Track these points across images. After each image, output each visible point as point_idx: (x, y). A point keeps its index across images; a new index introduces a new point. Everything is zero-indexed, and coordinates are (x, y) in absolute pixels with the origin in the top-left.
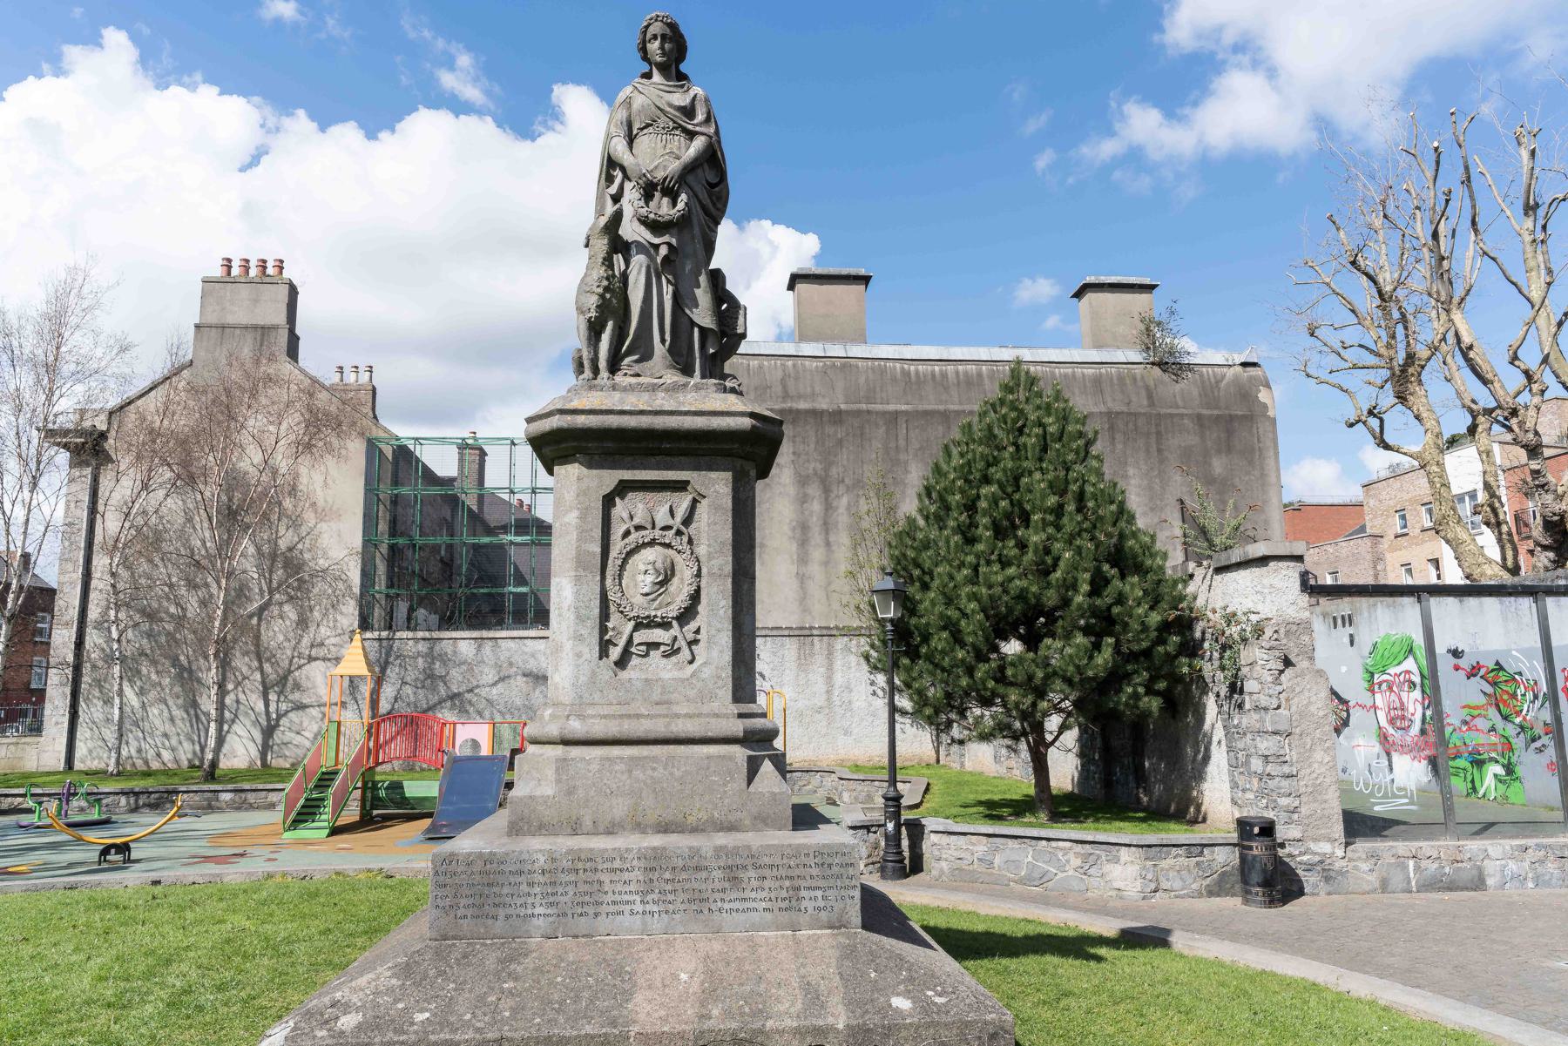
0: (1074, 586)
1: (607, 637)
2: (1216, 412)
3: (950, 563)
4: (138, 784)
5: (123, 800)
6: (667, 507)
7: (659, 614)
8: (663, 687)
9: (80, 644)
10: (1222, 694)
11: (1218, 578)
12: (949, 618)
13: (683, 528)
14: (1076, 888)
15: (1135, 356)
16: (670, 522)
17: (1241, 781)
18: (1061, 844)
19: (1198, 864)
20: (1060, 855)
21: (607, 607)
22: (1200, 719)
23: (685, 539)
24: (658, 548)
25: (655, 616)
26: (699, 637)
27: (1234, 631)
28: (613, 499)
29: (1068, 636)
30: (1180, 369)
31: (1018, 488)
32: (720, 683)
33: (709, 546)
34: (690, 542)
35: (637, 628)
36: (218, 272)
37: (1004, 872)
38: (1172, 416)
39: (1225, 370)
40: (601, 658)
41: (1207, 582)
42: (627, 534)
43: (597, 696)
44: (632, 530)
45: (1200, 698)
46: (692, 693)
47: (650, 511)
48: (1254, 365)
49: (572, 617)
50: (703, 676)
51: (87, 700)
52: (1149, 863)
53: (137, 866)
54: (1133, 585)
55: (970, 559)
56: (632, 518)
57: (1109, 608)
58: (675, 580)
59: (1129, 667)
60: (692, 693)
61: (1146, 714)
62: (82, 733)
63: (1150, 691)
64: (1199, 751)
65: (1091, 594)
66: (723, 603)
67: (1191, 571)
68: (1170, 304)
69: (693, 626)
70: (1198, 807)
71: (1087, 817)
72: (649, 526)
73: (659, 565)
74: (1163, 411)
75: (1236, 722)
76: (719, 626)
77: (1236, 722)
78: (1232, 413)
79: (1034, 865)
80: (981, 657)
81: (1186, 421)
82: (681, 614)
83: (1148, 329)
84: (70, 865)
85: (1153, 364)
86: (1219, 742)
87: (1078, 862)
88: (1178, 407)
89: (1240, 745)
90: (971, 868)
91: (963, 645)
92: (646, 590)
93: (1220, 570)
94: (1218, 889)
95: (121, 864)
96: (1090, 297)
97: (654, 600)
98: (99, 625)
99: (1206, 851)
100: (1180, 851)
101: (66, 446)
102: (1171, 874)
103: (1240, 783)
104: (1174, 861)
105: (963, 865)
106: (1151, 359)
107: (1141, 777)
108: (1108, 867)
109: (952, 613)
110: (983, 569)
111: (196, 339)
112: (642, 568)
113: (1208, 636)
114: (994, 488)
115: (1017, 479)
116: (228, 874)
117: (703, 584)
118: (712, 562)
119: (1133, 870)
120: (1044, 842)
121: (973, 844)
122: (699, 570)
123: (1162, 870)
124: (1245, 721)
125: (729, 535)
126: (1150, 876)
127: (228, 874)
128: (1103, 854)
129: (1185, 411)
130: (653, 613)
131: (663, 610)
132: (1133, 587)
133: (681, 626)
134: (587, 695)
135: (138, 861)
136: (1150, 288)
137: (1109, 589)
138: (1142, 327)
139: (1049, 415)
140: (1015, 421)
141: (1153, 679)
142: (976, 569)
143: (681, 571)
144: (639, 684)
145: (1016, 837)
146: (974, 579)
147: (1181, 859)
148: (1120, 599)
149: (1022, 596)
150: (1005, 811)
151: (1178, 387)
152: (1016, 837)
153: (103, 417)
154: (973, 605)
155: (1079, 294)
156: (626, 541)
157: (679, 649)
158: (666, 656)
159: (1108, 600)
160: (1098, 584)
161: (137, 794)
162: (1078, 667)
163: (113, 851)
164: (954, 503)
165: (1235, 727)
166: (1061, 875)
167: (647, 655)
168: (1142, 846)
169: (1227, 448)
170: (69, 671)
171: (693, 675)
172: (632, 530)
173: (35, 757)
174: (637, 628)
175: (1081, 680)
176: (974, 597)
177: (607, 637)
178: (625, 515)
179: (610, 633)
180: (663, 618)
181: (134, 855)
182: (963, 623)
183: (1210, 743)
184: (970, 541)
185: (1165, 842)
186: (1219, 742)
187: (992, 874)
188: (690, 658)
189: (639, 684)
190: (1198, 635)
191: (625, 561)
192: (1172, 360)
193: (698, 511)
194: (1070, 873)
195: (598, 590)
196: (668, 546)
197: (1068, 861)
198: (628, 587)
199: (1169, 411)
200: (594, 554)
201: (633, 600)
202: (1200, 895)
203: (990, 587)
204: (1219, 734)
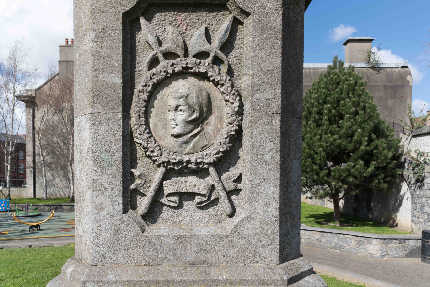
0: (360, 143)
1: (133, 187)
2: (391, 84)
3: (311, 133)
4: (50, 203)
5: (47, 208)
6: (203, 29)
7: (193, 159)
8: (198, 245)
9: (34, 161)
10: (412, 183)
11: (414, 139)
12: (310, 154)
13: (221, 55)
14: (354, 252)
15: (364, 65)
16: (206, 47)
17: (417, 215)
18: (349, 236)
19: (403, 246)
20: (348, 240)
21: (134, 151)
22: (399, 190)
23: (224, 69)
24: (192, 80)
25: (189, 162)
26: (240, 186)
27: (422, 159)
28: (138, 19)
29: (355, 161)
30: (380, 69)
31: (338, 105)
32: (265, 241)
33: (254, 76)
34: (230, 72)
35: (166, 176)
36: (64, 43)
37: (326, 245)
38: (375, 86)
39: (395, 69)
40: (125, 211)
41: (408, 141)
42: (154, 62)
43: (122, 255)
44: (160, 57)
45: (400, 183)
46: (232, 252)
47: (182, 34)
48: (406, 67)
49: (91, 163)
50: (246, 232)
51: (38, 177)
52: (384, 245)
53: (42, 232)
54: (382, 142)
55: (319, 132)
56: (160, 43)
57: (372, 150)
58: (212, 119)
59: (377, 173)
60: (232, 252)
61: (383, 189)
62: (37, 186)
63: (385, 182)
64: (397, 202)
65: (368, 145)
66: (269, 146)
67: (401, 136)
68: (378, 45)
69: (233, 173)
70: (394, 221)
71: (353, 223)
72: (181, 53)
73: (193, 99)
74: (373, 84)
75: (417, 193)
76: (265, 173)
77: (417, 193)
78: (397, 84)
79: (338, 243)
80: (321, 168)
81: (380, 87)
82: (219, 159)
83: (369, 55)
84: (22, 231)
85: (370, 68)
86: (408, 199)
87: (355, 243)
88: (378, 83)
89: (419, 201)
90: (313, 242)
91: (316, 164)
92: (177, 130)
93: (414, 136)
94: (411, 254)
95: (36, 231)
96: (350, 44)
97: (187, 142)
98: (39, 155)
99: (406, 241)
100: (394, 241)
101: (23, 101)
102: (392, 249)
103: (417, 215)
104: (394, 244)
105: (310, 241)
106: (370, 66)
107: (369, 209)
108: (367, 246)
109: (312, 152)
110: (325, 136)
111: (59, 66)
112: (173, 103)
113: (407, 161)
114: (329, 105)
115: (338, 101)
116: (55, 243)
117: (246, 123)
118: (258, 96)
119: (377, 247)
120: (342, 235)
121: (314, 234)
122: (241, 106)
123: (389, 248)
124: (422, 193)
125: (278, 62)
126: (384, 250)
127: (55, 243)
128: (366, 241)
129: (380, 84)
130: (186, 158)
131: (199, 155)
132: (381, 142)
133: (219, 174)
134: (109, 254)
135: (42, 230)
136: (370, 41)
137: (373, 143)
138: (367, 54)
139: (350, 77)
140: (336, 79)
141: (385, 177)
142: (321, 135)
143: (220, 107)
144: (170, 242)
145: (331, 233)
146: (320, 140)
147: (396, 244)
148: (376, 147)
149: (339, 146)
150: (322, 220)
151: (378, 76)
152: (331, 233)
153: (34, 91)
154: (321, 149)
155: (345, 44)
156: (154, 70)
157: (217, 200)
158: (202, 207)
159: (372, 148)
160: (370, 141)
161: (50, 206)
162: (360, 172)
163: (34, 227)
164: (313, 111)
165: (417, 195)
166: (348, 247)
167: (180, 206)
168: (382, 239)
169: (394, 96)
170: (32, 169)
171: (234, 230)
172: (160, 57)
173: (25, 194)
174: (166, 176)
175: (360, 177)
176: (321, 146)
177: (133, 187)
178: (152, 39)
179: (137, 182)
180: (197, 164)
181: (41, 228)
182: (315, 156)
183: (402, 199)
184: (318, 126)
185: (391, 238)
186: (408, 199)
187: (321, 245)
188: (229, 211)
189: (170, 242)
190: (402, 160)
191: (152, 96)
192: (377, 66)
193: (239, 35)
194: (352, 246)
195: (120, 130)
196: (203, 76)
197: (351, 242)
198: (156, 126)
199: (375, 84)
200: (114, 85)
201: (162, 143)
202: (402, 257)
203: (327, 143)
204: (408, 195)
